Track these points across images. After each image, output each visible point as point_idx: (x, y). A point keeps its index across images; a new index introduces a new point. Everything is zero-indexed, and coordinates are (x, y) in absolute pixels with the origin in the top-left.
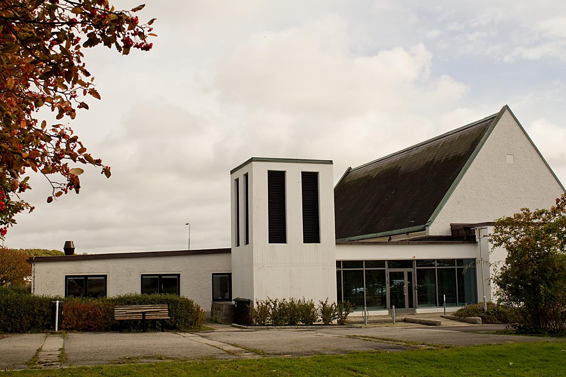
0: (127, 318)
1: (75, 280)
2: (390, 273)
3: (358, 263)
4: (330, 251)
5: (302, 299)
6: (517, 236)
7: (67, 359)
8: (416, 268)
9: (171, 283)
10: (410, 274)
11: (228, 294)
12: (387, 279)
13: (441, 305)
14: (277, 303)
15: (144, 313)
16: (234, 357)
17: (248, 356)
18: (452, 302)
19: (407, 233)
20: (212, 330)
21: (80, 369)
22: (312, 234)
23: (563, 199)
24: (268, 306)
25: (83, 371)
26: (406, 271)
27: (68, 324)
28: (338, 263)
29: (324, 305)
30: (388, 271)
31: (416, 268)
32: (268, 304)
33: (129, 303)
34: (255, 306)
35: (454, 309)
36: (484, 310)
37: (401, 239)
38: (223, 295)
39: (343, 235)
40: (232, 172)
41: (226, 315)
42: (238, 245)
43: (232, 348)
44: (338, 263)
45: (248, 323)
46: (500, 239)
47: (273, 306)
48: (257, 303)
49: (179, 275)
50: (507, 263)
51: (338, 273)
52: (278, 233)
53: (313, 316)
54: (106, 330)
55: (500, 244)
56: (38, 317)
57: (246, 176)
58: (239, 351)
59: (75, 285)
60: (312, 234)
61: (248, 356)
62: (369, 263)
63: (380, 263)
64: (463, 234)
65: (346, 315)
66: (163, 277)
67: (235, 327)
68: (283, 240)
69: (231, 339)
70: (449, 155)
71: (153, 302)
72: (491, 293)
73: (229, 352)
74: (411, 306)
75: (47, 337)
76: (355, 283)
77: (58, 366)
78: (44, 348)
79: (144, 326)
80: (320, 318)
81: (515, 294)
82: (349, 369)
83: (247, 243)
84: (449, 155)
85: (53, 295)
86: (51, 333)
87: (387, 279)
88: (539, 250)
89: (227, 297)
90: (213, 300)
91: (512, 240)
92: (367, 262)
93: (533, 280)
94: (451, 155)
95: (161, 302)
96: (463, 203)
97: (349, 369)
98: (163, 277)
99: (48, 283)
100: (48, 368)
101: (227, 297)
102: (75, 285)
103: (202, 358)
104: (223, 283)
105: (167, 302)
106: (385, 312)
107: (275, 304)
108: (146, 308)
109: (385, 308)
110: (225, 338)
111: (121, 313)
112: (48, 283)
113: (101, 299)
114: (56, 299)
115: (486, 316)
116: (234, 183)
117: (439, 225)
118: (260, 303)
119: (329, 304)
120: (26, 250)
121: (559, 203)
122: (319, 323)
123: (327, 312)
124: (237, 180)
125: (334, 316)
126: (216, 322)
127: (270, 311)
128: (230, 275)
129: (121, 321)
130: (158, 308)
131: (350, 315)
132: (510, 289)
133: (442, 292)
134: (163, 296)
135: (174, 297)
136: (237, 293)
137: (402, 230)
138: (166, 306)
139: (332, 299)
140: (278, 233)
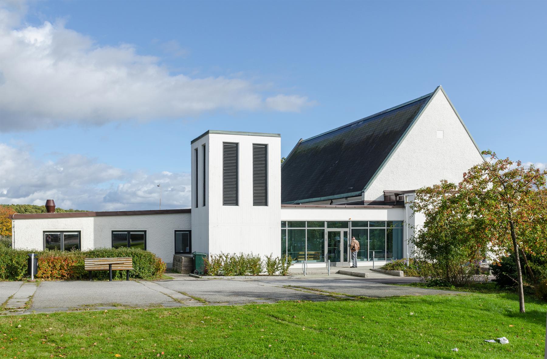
0: (96, 268)
1: (52, 235)
2: (330, 233)
3: (301, 224)
4: (278, 213)
5: (250, 253)
6: (435, 203)
7: (32, 306)
8: (351, 228)
9: (137, 239)
10: (345, 233)
11: (188, 248)
12: (326, 237)
13: (372, 259)
14: (229, 257)
15: (110, 265)
16: (178, 304)
17: (192, 303)
18: (381, 258)
19: (346, 198)
20: (171, 279)
21: (40, 316)
22: (261, 198)
23: (469, 173)
24: (221, 259)
25: (43, 317)
26: (342, 230)
27: (44, 273)
28: (283, 224)
29: (269, 259)
30: (327, 230)
31: (351, 228)
32: (221, 257)
33: (98, 256)
34: (210, 259)
35: (382, 263)
36: (406, 264)
37: (99, 263)
38: (184, 249)
39: (290, 197)
40: (192, 142)
41: (185, 267)
42: (197, 207)
43: (180, 296)
44: (283, 224)
45: (206, 273)
46: (419, 206)
47: (225, 259)
48: (212, 256)
49: (145, 231)
50: (425, 227)
51: (283, 232)
52: (231, 197)
53: (260, 268)
54: (78, 279)
55: (420, 210)
56: (18, 268)
57: (204, 146)
58: (183, 299)
59: (52, 240)
60: (261, 198)
61: (192, 303)
62: (311, 224)
63: (321, 224)
64: (393, 200)
65: (288, 267)
66: (131, 233)
67: (192, 276)
68: (265, 203)
69: (183, 288)
70: (387, 130)
71: (119, 255)
72: (412, 252)
73: (175, 300)
74: (345, 260)
75: (23, 285)
76: (299, 241)
77: (22, 312)
78: (15, 296)
79: (106, 275)
80: (265, 270)
81: (431, 253)
82: (273, 316)
83: (204, 205)
84: (387, 130)
85: (30, 249)
86: (28, 281)
87: (326, 237)
88: (453, 216)
89: (188, 250)
90: (176, 253)
91: (430, 207)
92: (308, 222)
93: (446, 242)
94: (389, 130)
95: (127, 255)
96: (396, 174)
97: (273, 316)
98: (131, 233)
99: (28, 236)
100: (13, 314)
101: (188, 250)
102: (52, 240)
103: (151, 305)
104: (184, 240)
105: (133, 255)
106: (323, 265)
107: (226, 257)
108: (112, 260)
109: (323, 261)
110: (183, 285)
111: (90, 264)
112: (28, 236)
113: (73, 252)
114: (32, 252)
115: (408, 270)
116: (194, 152)
117: (374, 191)
118: (213, 257)
119: (273, 258)
120: (17, 205)
121: (466, 177)
122: (265, 274)
123: (272, 265)
124: (197, 150)
125: (277, 268)
126: (176, 271)
127: (223, 264)
128: (190, 231)
129: (90, 271)
130: (122, 260)
131: (291, 267)
132: (426, 248)
133: (373, 248)
134: (129, 250)
135: (139, 250)
136: (196, 248)
137: (342, 195)
138: (131, 259)
139: (276, 253)
140: (231, 197)
